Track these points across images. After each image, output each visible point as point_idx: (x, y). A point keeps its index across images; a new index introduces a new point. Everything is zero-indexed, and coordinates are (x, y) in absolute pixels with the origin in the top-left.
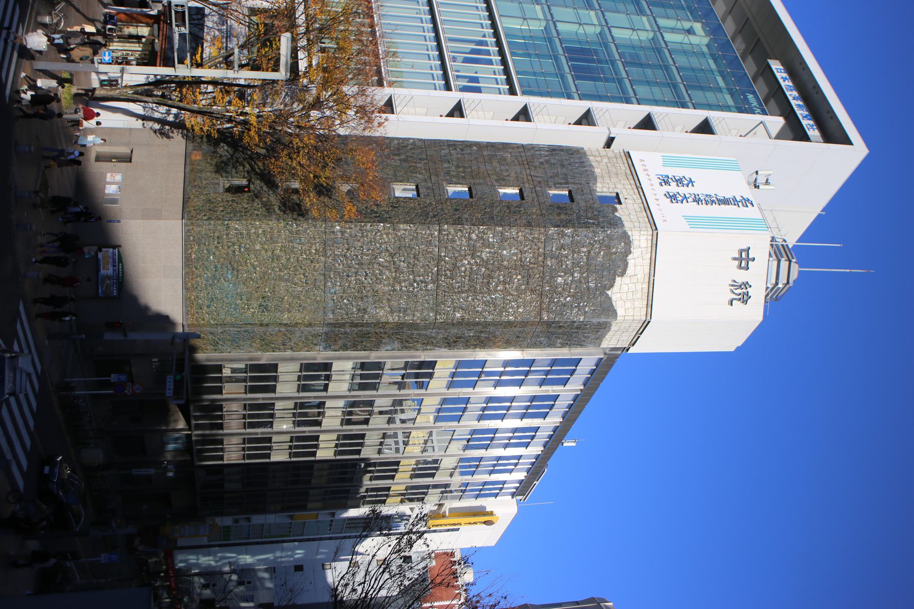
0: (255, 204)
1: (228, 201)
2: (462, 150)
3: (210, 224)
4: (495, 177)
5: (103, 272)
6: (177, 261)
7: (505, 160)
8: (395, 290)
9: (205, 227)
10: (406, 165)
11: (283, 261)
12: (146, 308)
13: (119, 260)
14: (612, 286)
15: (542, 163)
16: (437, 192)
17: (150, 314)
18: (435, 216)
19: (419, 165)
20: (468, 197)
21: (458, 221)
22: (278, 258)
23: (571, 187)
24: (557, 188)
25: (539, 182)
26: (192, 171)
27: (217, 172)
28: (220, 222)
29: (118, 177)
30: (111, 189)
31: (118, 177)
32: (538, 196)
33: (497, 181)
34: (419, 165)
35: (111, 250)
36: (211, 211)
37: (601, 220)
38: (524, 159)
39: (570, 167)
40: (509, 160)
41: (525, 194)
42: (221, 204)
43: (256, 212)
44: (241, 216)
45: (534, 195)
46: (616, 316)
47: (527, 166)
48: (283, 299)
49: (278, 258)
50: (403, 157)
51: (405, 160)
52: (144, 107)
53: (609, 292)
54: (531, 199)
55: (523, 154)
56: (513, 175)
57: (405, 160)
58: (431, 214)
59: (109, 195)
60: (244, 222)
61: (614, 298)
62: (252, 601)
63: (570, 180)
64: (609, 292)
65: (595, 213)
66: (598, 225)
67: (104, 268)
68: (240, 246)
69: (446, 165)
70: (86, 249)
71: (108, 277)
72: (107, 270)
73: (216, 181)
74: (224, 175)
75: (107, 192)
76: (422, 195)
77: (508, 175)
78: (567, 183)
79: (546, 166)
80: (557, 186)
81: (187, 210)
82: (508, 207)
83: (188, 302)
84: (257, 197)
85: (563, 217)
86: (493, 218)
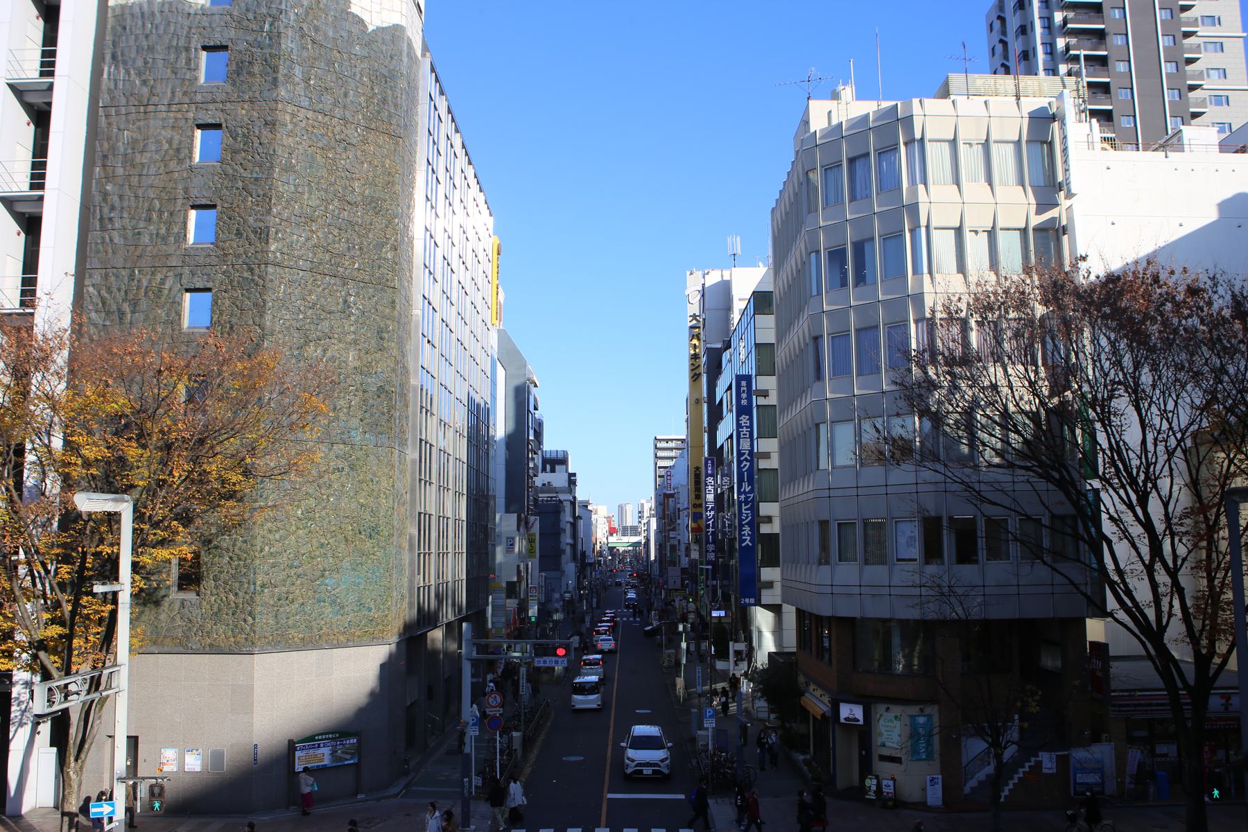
0: (224, 545)
1: (216, 587)
2: (113, 208)
3: (260, 613)
4: (173, 165)
5: (326, 761)
6: (311, 657)
7: (135, 141)
8: (355, 342)
9: (265, 621)
10: (144, 305)
11: (312, 502)
12: (372, 694)
13: (311, 740)
14: (361, 21)
15: (144, 82)
16: (201, 260)
17: (377, 690)
18: (251, 270)
19: (145, 283)
20: (211, 214)
21: (263, 235)
22: (309, 510)
23: (196, 42)
24: (197, 68)
25: (185, 93)
26: (155, 643)
27: (157, 603)
28: (258, 598)
29: (169, 754)
30: (194, 763)
31: (169, 754)
32: (214, 102)
33: (180, 161)
34: (145, 283)
35: (298, 754)
36: (245, 610)
37: (264, 10)
38: (133, 109)
39: (154, 37)
40: (136, 135)
41: (210, 121)
42: (223, 595)
43: (239, 544)
44: (245, 566)
45: (211, 106)
46: (402, 27)
47: (151, 108)
48: (362, 506)
49: (309, 510)
50: (126, 307)
51: (135, 305)
52: (21, 724)
53: (371, 28)
54: (219, 114)
55: (123, 110)
56: (168, 133)
57: (135, 305)
58: (246, 275)
59: (203, 765)
60: (257, 562)
61: (379, 24)
62: (513, 539)
63: (182, 43)
64: (371, 28)
65: (251, 16)
66: (275, 19)
67: (321, 760)
68: (291, 567)
69: (146, 239)
70: (307, 790)
71: (333, 752)
72: (324, 755)
73: (177, 605)
74: (163, 592)
75: (198, 769)
76: (209, 285)
77: (170, 142)
78: (187, 49)
79: (147, 75)
80: (191, 66)
81: (242, 645)
82: (235, 152)
83: (373, 639)
84: (210, 542)
85: (256, 69)
86: (256, 179)
